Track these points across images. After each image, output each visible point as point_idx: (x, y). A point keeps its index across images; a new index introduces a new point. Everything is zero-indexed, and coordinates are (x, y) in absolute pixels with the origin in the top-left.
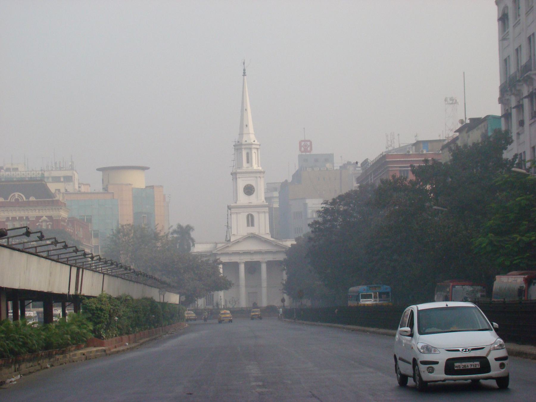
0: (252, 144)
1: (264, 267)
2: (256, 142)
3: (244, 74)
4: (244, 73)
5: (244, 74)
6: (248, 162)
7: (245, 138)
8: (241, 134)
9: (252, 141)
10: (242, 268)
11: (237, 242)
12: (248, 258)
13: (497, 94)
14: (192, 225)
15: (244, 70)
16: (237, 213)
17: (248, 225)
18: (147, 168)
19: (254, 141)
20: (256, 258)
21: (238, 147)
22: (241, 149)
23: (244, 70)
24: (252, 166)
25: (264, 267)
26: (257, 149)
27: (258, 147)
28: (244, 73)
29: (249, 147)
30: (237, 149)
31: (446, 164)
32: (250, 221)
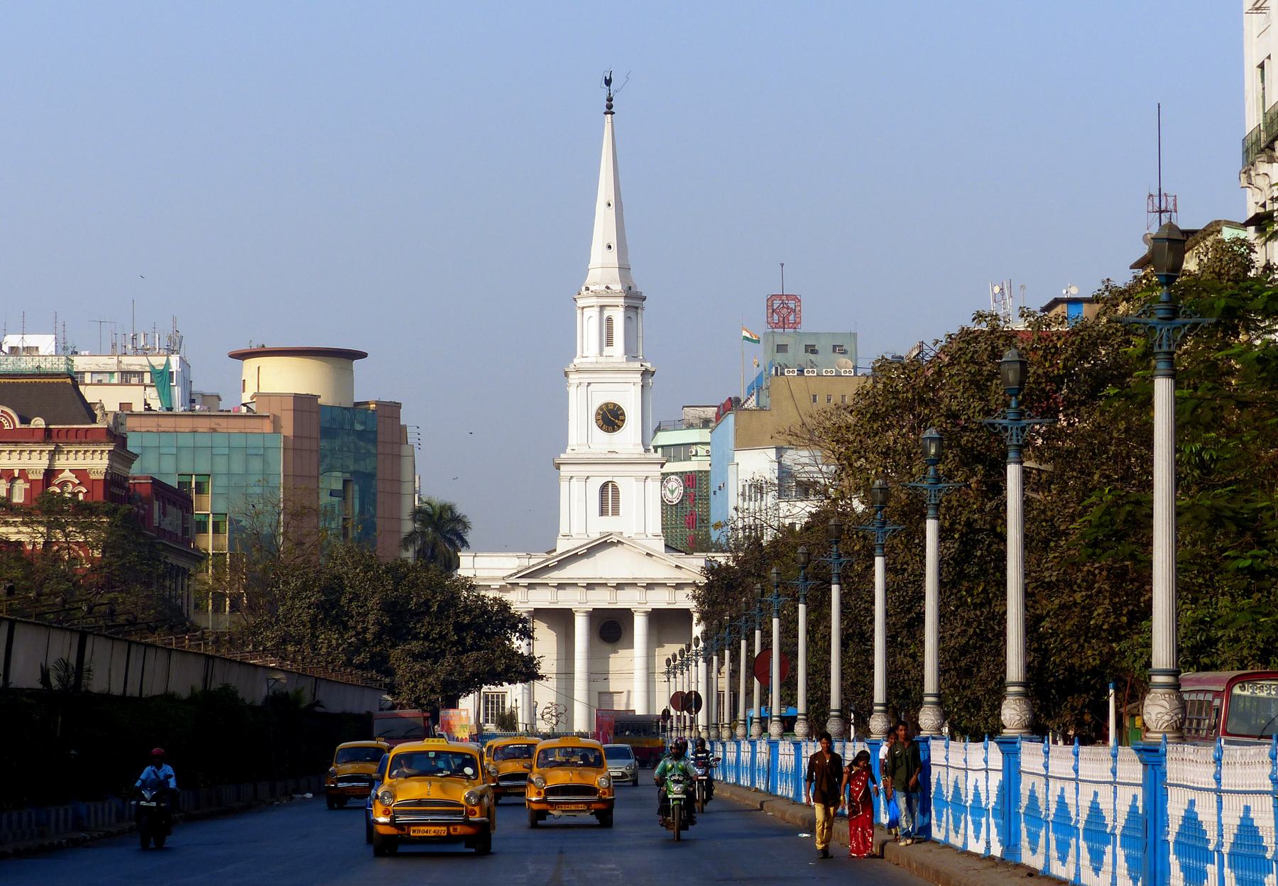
1: (640, 624)
4: (610, 107)
6: (609, 320)
10: (581, 625)
11: (574, 557)
12: (602, 599)
15: (610, 100)
17: (603, 512)
20: (623, 600)
23: (610, 100)
25: (640, 624)
28: (610, 107)
32: (608, 498)
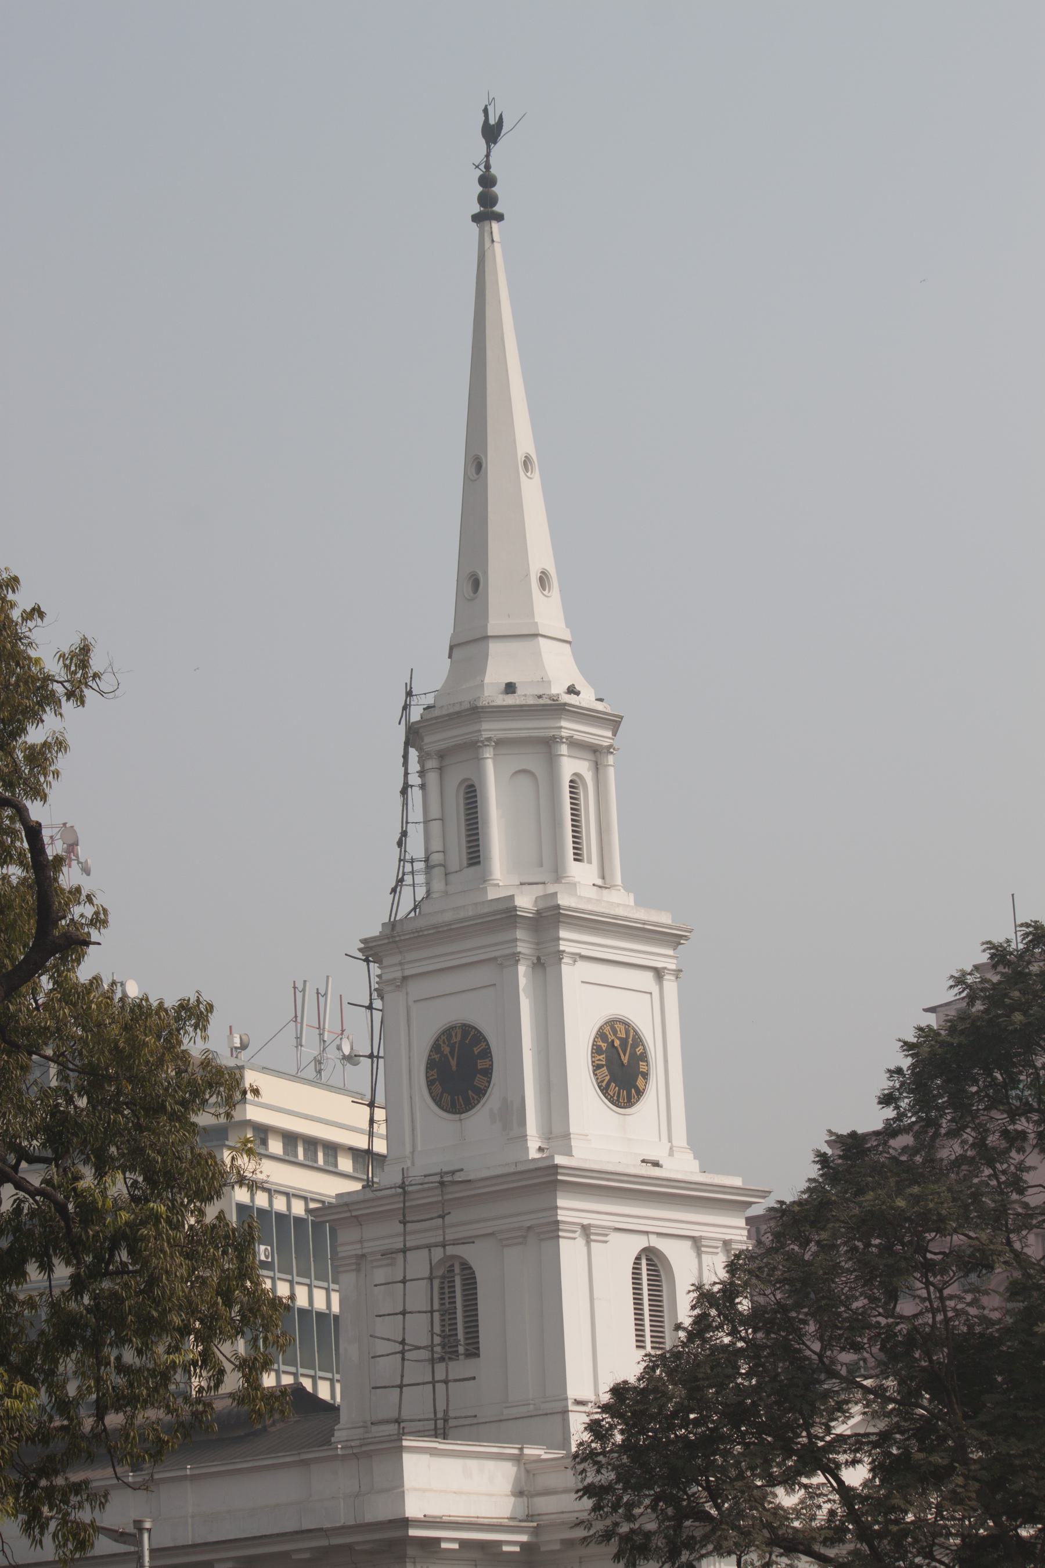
0: (556, 709)
2: (587, 698)
3: (487, 212)
4: (487, 200)
5: (487, 212)
7: (500, 668)
8: (469, 644)
9: (558, 688)
13: (478, 1275)
14: (812, 1157)
15: (487, 181)
16: (586, 1229)
18: (99, 944)
19: (572, 690)
21: (447, 739)
22: (472, 748)
23: (487, 181)
24: (484, 878)
26: (596, 753)
27: (601, 735)
28: (487, 200)
29: (538, 725)
30: (442, 755)
31: (56, 880)
